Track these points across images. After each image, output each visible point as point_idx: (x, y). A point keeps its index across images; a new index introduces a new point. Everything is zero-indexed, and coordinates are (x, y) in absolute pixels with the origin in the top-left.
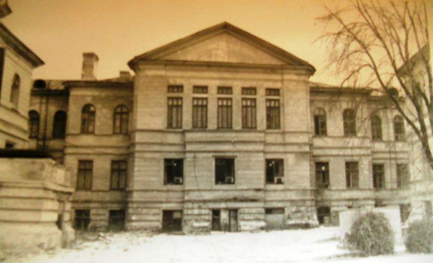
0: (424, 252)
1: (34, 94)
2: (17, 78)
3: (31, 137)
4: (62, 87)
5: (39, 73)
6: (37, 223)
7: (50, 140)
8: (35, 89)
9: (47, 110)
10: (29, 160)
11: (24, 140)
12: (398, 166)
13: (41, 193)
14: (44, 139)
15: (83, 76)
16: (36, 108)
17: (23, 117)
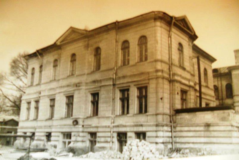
0: (54, 65)
1: (214, 76)
2: (205, 70)
3: (216, 99)
4: (227, 71)
5: (215, 65)
6: (231, 143)
7: (225, 99)
8: (214, 74)
9: (221, 84)
10: (221, 112)
11: (214, 101)
12: (175, 115)
13: (230, 128)
14: (222, 99)
15: (236, 63)
16: (216, 83)
17: (211, 89)
